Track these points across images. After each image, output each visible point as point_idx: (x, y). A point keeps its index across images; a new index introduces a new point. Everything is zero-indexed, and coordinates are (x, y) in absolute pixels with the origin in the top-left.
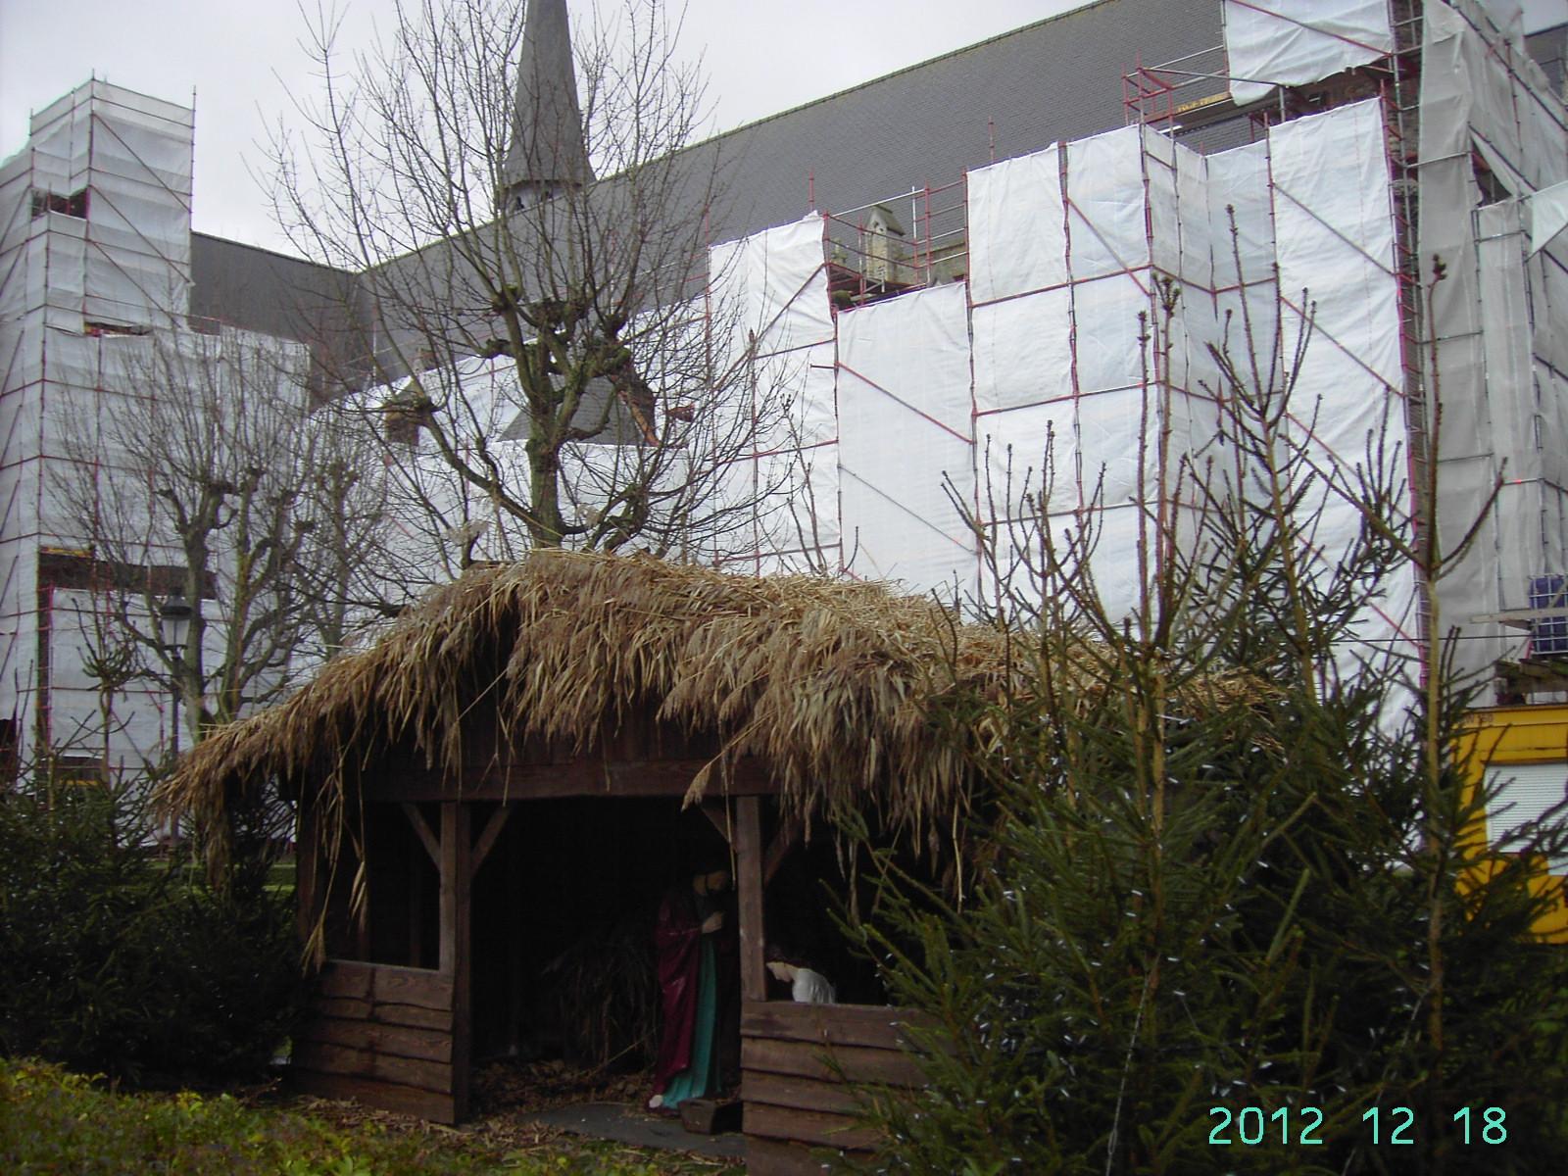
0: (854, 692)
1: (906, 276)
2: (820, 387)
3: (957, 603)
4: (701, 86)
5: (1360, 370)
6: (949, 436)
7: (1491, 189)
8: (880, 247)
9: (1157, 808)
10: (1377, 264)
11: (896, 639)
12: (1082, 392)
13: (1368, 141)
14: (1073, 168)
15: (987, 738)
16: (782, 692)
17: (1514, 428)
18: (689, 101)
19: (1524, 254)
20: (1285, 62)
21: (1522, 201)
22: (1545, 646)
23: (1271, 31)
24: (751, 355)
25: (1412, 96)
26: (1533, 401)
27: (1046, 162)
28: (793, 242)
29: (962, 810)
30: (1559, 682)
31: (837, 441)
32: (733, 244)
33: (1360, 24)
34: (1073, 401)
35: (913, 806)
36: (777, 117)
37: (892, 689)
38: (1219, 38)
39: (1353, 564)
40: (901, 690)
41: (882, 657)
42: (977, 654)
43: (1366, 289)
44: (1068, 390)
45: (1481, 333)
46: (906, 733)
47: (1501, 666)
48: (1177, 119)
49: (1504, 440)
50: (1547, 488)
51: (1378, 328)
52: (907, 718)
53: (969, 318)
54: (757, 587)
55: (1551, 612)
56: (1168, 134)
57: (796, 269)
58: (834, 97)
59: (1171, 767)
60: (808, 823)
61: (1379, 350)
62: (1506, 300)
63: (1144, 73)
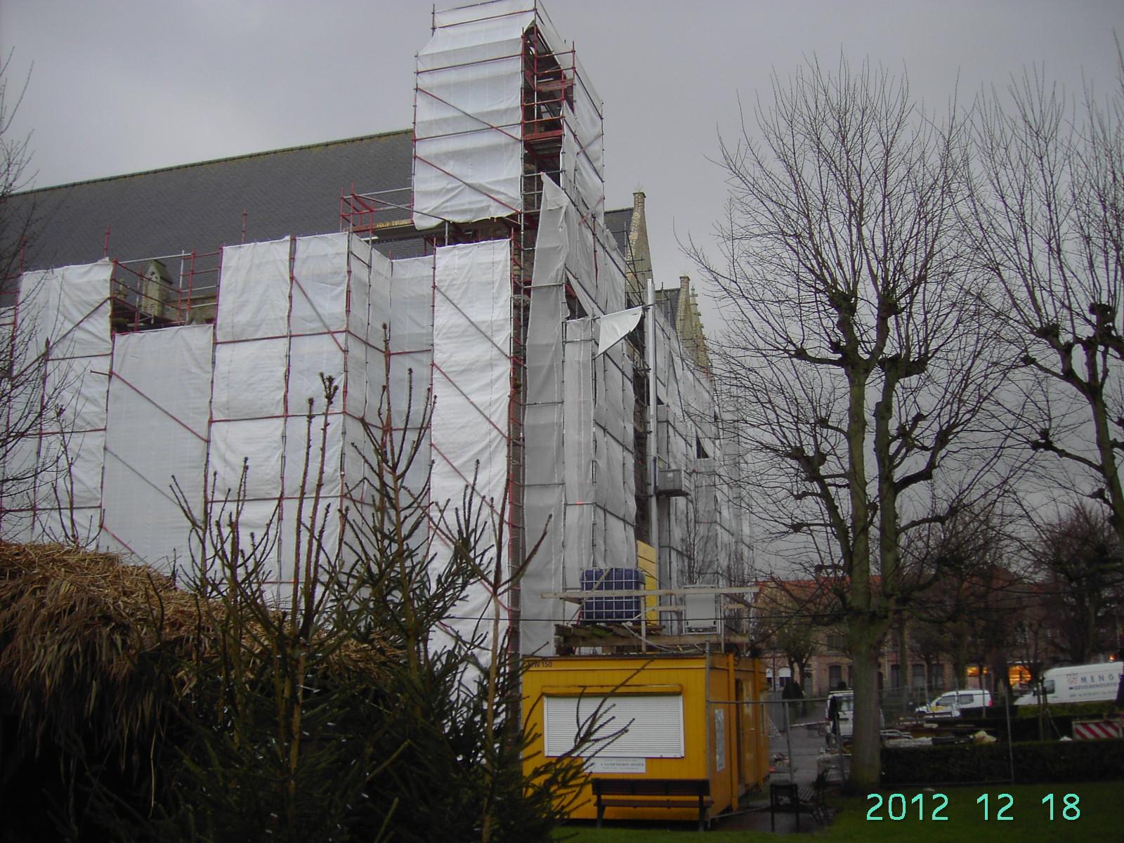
0: (82, 646)
1: (171, 314)
2: (97, 389)
3: (174, 574)
4: (25, 159)
5: (481, 418)
6: (190, 434)
7: (576, 310)
8: (154, 290)
9: (294, 752)
10: (499, 349)
11: (119, 606)
12: (290, 413)
13: (501, 267)
14: (298, 255)
15: (182, 684)
16: (25, 643)
17: (579, 467)
18: (14, 169)
19: (593, 354)
20: (451, 206)
21: (594, 320)
22: (590, 615)
23: (444, 183)
24: (45, 357)
25: (531, 241)
26: (592, 451)
27: (280, 249)
28: (86, 279)
29: (159, 737)
30: (596, 641)
31: (105, 429)
32: (41, 272)
33: (502, 190)
34: (283, 419)
35: (121, 733)
36: (88, 183)
37: (113, 644)
38: (410, 183)
39: (447, 578)
40: (119, 643)
41: (106, 619)
42: (181, 620)
43: (491, 365)
44: (280, 411)
45: (562, 402)
46: (119, 679)
47: (561, 630)
48: (375, 232)
49: (573, 473)
50: (598, 509)
51: (495, 392)
52: (122, 667)
53: (214, 351)
54: (17, 554)
55: (594, 593)
56: (367, 242)
57: (86, 298)
58: (133, 176)
59: (306, 723)
60: (38, 743)
61: (495, 407)
62: (580, 383)
63: (355, 197)
